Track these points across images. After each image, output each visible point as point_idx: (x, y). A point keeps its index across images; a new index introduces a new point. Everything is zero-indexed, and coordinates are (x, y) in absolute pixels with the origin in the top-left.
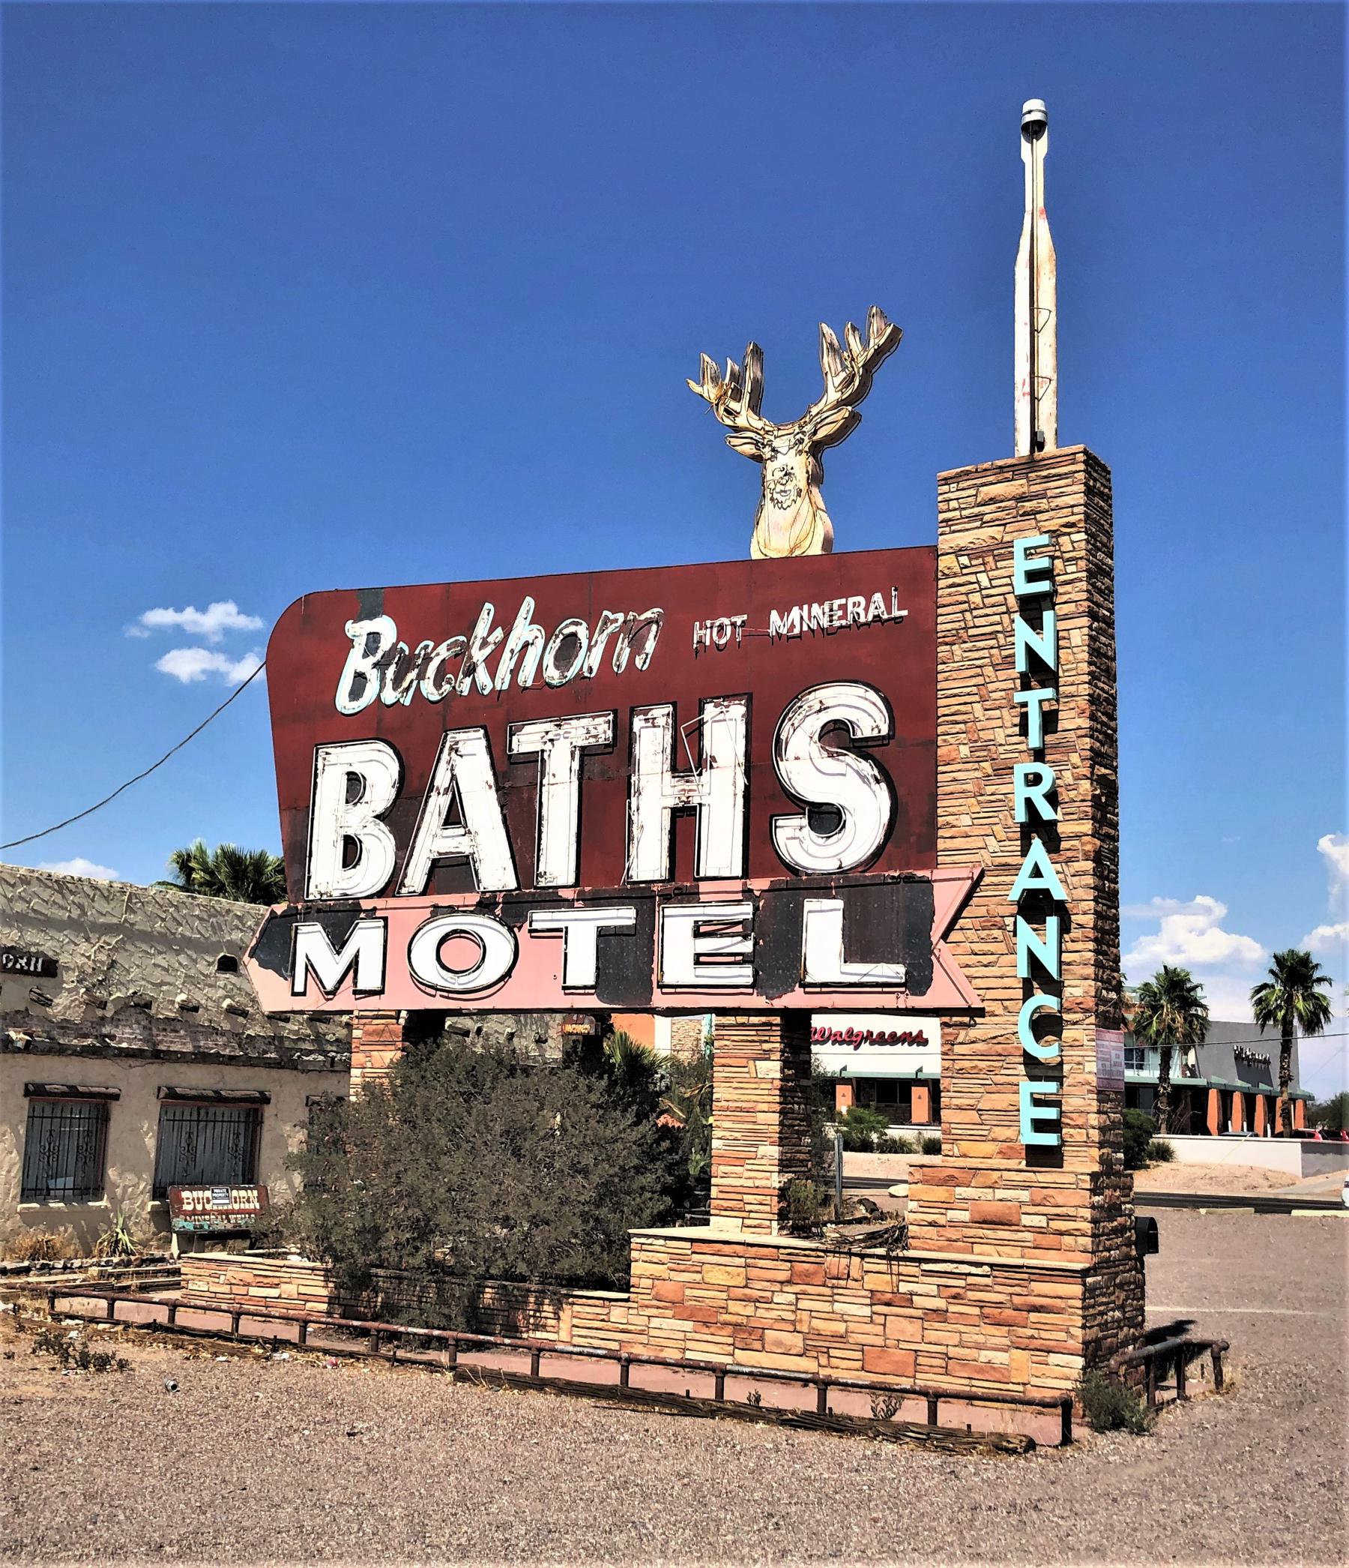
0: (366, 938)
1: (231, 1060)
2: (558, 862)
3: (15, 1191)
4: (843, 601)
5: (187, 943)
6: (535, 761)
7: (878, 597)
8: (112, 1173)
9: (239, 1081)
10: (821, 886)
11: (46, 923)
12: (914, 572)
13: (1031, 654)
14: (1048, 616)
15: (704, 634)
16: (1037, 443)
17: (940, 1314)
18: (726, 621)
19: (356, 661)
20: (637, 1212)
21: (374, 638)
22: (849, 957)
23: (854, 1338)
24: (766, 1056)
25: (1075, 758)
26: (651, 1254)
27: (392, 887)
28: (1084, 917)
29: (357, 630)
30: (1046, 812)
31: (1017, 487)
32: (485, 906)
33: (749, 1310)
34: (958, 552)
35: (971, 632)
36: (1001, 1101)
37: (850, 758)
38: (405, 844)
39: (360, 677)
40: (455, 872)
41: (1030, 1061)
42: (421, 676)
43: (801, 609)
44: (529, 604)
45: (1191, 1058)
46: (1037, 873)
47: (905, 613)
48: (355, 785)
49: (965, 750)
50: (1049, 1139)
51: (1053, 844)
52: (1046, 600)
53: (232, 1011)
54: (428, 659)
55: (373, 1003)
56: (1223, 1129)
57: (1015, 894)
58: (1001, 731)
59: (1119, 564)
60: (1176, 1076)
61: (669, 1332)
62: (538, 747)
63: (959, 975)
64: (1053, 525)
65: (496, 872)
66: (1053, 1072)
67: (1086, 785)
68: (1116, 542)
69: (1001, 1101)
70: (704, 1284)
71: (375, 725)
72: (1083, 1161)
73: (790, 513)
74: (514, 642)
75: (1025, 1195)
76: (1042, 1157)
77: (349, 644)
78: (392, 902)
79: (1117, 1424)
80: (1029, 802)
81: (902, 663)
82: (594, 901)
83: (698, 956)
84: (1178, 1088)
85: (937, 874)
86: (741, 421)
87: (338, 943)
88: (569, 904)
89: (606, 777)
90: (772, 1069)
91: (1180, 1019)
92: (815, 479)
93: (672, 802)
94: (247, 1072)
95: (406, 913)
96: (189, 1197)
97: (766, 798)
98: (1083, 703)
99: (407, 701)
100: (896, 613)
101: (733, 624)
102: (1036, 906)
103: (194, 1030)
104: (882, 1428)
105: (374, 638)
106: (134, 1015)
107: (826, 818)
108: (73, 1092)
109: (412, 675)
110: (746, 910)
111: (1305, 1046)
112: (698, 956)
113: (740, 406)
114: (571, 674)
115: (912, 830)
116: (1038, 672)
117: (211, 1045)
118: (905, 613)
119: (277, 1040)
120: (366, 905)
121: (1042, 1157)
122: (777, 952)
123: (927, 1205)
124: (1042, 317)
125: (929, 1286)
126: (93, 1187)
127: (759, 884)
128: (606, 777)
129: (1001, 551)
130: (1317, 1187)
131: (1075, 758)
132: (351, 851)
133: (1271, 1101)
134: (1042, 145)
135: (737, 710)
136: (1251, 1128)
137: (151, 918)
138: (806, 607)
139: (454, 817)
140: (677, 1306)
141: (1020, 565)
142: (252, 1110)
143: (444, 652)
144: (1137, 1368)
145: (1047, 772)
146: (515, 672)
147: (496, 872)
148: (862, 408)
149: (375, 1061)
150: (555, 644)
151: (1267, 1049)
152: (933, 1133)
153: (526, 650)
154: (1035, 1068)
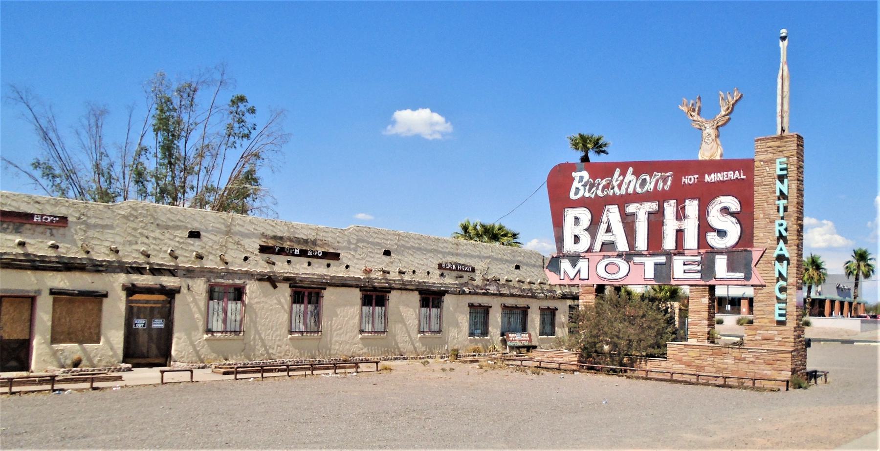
0: (582, 264)
1: (520, 296)
2: (641, 243)
3: (467, 334)
5: (507, 261)
8: (490, 329)
9: (521, 302)
10: (720, 252)
11: (472, 256)
12: (747, 166)
13: (781, 191)
14: (786, 181)
15: (686, 180)
16: (783, 130)
19: (576, 184)
20: (668, 338)
21: (581, 178)
22: (728, 271)
25: (792, 219)
26: (672, 349)
27: (590, 250)
28: (794, 261)
29: (576, 175)
30: (784, 233)
31: (778, 143)
32: (620, 256)
33: (700, 362)
34: (760, 161)
36: (769, 309)
37: (729, 217)
38: (593, 237)
39: (577, 189)
40: (608, 246)
41: (778, 299)
42: (597, 189)
44: (631, 170)
45: (819, 289)
46: (781, 249)
49: (761, 216)
50: (783, 318)
51: (786, 241)
52: (786, 176)
53: (519, 281)
54: (599, 184)
55: (586, 282)
56: (831, 314)
57: (775, 255)
58: (772, 211)
59: (805, 164)
60: (813, 295)
61: (678, 367)
62: (634, 211)
63: (759, 276)
64: (788, 155)
66: (785, 301)
67: (795, 226)
68: (805, 158)
69: (769, 309)
70: (688, 356)
72: (791, 324)
73: (710, 146)
74: (626, 180)
75: (776, 332)
76: (781, 323)
77: (573, 179)
78: (590, 254)
79: (800, 387)
80: (780, 232)
81: (744, 191)
82: (653, 255)
84: (814, 300)
85: (753, 249)
86: (695, 118)
87: (574, 265)
88: (645, 255)
90: (706, 301)
91: (816, 274)
92: (718, 136)
93: (677, 228)
94: (523, 299)
95: (595, 257)
96: (511, 336)
97: (704, 228)
98: (795, 204)
99: (593, 196)
102: (781, 258)
103: (509, 287)
104: (741, 386)
105: (581, 178)
106: (494, 283)
107: (722, 233)
108: (480, 306)
109: (594, 189)
110: (699, 258)
111: (864, 283)
113: (695, 114)
114: (645, 190)
115: (746, 238)
116: (783, 196)
117: (514, 292)
119: (530, 290)
120: (582, 255)
121: (781, 323)
122: (708, 269)
123: (749, 335)
124: (785, 94)
125: (751, 355)
126: (485, 333)
127: (702, 251)
129: (772, 162)
130: (866, 335)
131: (792, 219)
132: (577, 239)
133: (850, 304)
134: (786, 42)
135: (696, 203)
136: (842, 314)
137: (497, 254)
139: (609, 230)
140: (680, 362)
141: (778, 166)
142: (525, 311)
143: (604, 182)
144: (804, 377)
145: (784, 222)
146: (627, 189)
147: (622, 246)
148: (731, 116)
149: (587, 300)
150: (639, 182)
151: (849, 284)
152: (751, 317)
153: (630, 183)
154: (779, 300)
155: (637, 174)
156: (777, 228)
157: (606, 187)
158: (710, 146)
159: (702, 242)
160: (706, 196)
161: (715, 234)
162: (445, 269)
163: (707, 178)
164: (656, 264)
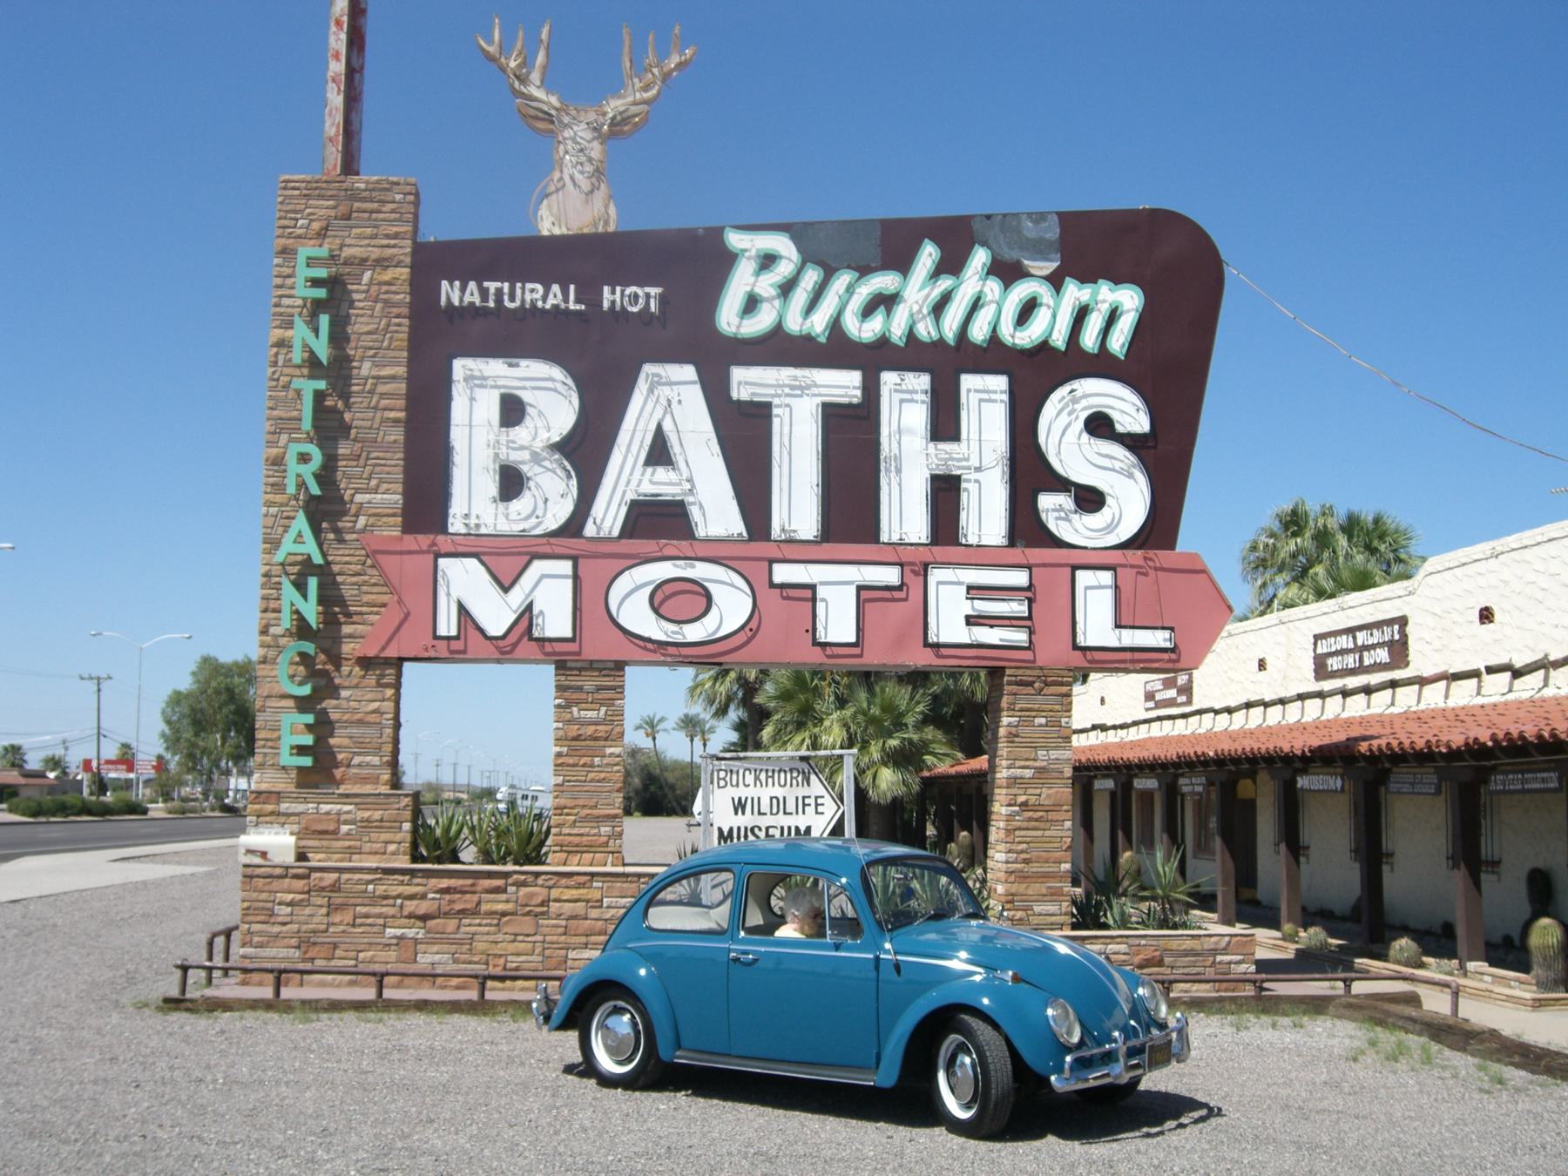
2: (798, 504)
6: (760, 413)
7: (556, 288)
18: (640, 291)
23: (484, 907)
40: (658, 522)
48: (512, 411)
77: (728, 259)
89: (851, 441)
97: (1029, 472)
100: (572, 306)
101: (648, 296)
107: (1089, 499)
132: (511, 483)
139: (659, 453)
147: (718, 513)
159: (1026, 527)
163: (610, 297)
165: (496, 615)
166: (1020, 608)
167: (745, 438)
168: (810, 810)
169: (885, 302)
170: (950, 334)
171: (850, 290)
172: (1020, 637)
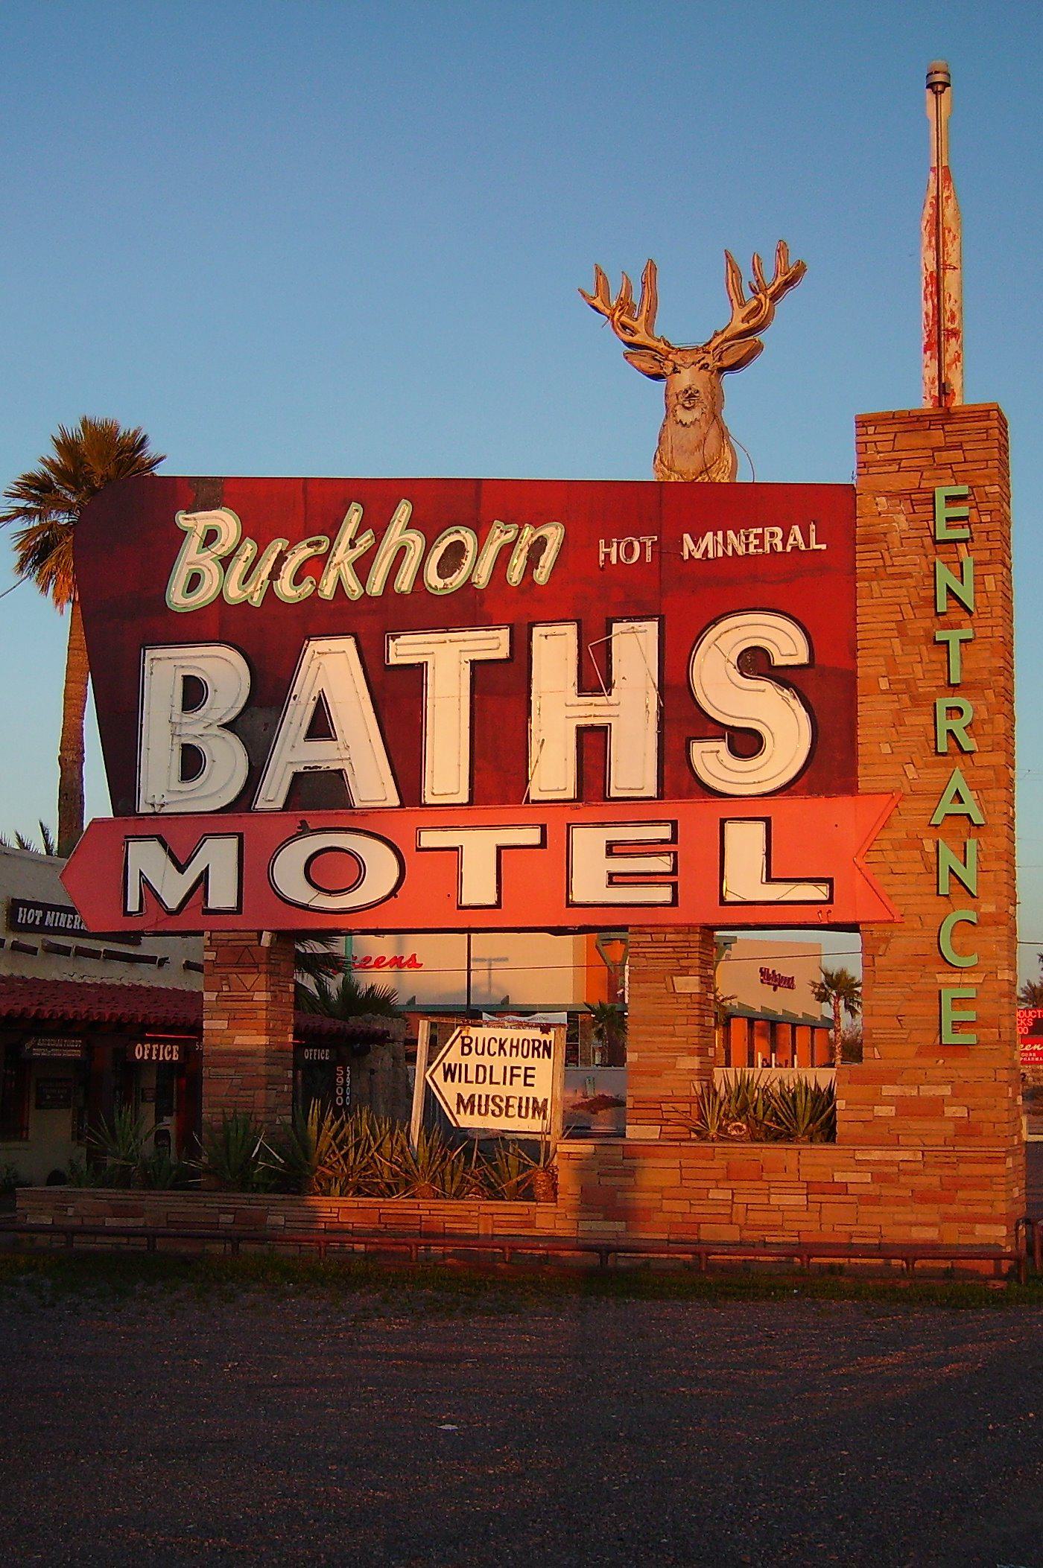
2: (447, 772)
4: (759, 531)
5: (643, 1073)
6: (417, 672)
17: (875, 1200)
19: (191, 556)
24: (684, 972)
29: (194, 522)
35: (890, 570)
43: (715, 534)
44: (404, 510)
46: (958, 797)
47: (824, 547)
48: (194, 693)
65: (372, 783)
71: (220, 623)
75: (947, 1091)
83: (611, 875)
89: (501, 691)
97: (681, 718)
99: (256, 600)
100: (814, 546)
105: (211, 536)
107: (746, 743)
112: (611, 875)
118: (824, 547)
128: (501, 691)
132: (192, 762)
138: (720, 533)
139: (320, 727)
147: (372, 783)
155: (429, 525)
156: (944, 724)
157: (314, 567)
158: (693, 433)
159: (676, 776)
160: (686, 610)
161: (722, 746)
162: (526, 1076)
164: (500, 849)
165: (173, 889)
166: (663, 864)
167: (398, 699)
168: (519, 1081)
169: (314, 567)
170: (376, 588)
171: (281, 558)
172: (664, 894)
